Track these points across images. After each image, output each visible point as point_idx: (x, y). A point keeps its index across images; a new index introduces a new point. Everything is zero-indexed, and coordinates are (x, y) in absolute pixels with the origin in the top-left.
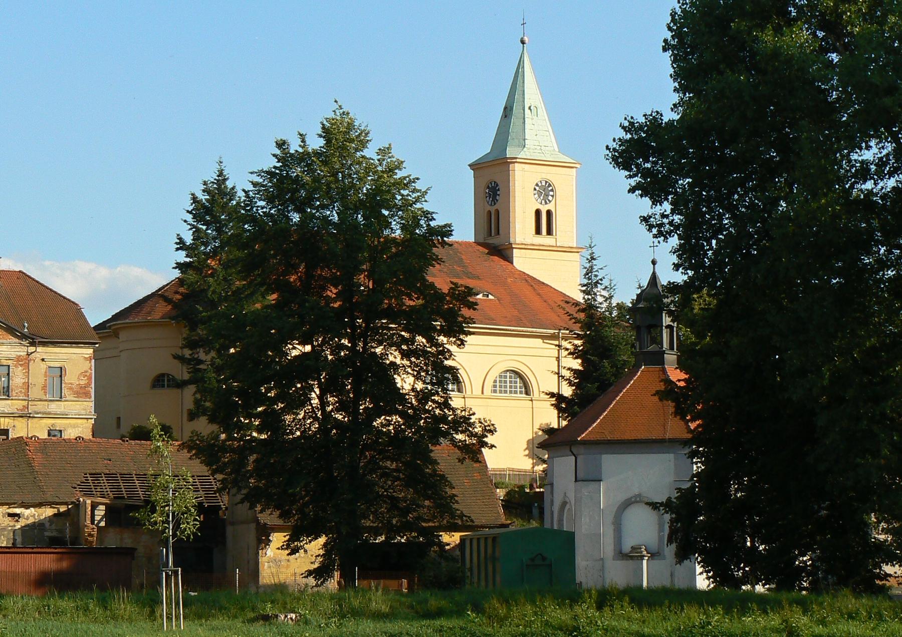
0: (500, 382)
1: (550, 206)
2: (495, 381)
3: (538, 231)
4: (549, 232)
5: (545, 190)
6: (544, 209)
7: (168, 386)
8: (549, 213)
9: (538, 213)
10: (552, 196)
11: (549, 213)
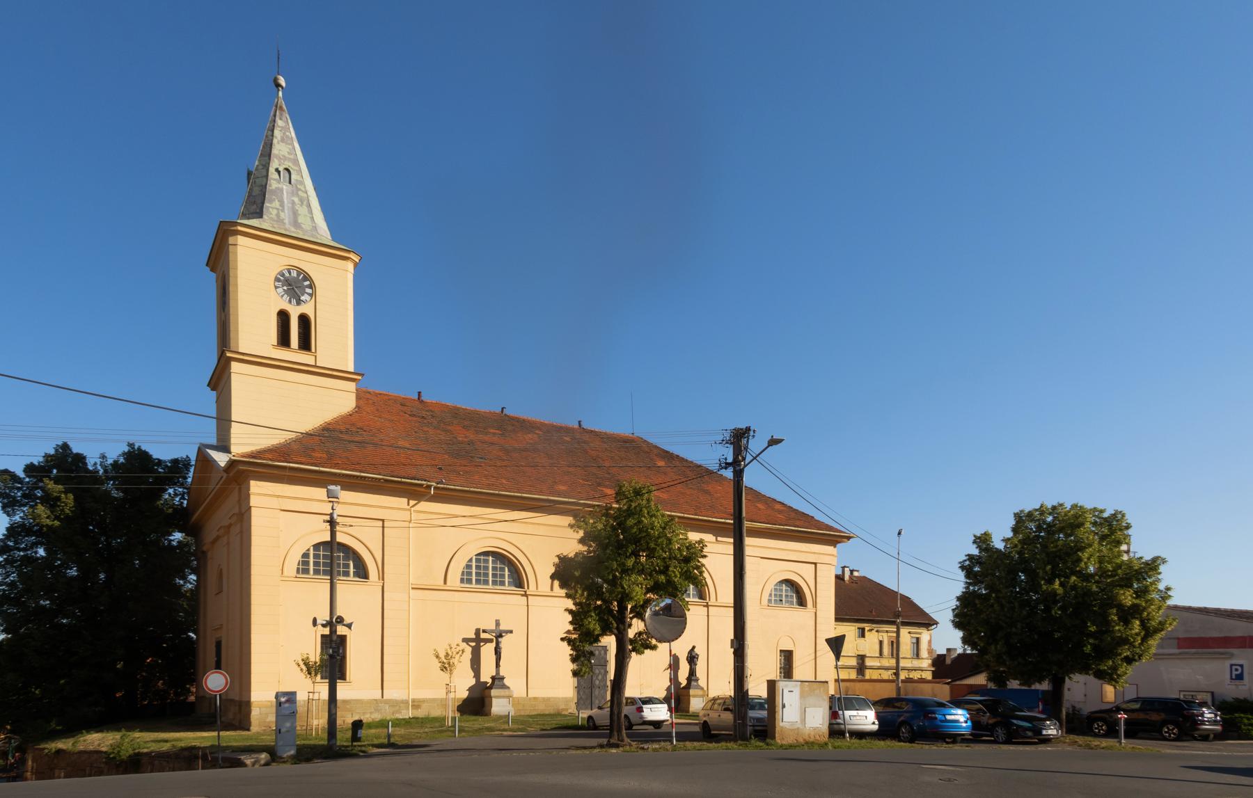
0: (478, 567)
1: (307, 309)
2: (469, 566)
3: (284, 340)
4: (305, 344)
5: (296, 284)
6: (294, 313)
7: (478, 582)
8: (304, 321)
9: (283, 317)
10: (311, 295)
11: (304, 321)
